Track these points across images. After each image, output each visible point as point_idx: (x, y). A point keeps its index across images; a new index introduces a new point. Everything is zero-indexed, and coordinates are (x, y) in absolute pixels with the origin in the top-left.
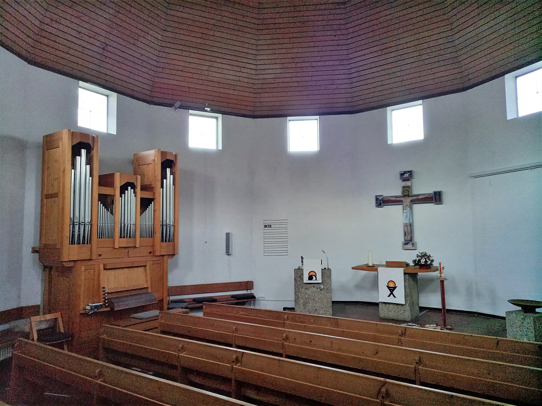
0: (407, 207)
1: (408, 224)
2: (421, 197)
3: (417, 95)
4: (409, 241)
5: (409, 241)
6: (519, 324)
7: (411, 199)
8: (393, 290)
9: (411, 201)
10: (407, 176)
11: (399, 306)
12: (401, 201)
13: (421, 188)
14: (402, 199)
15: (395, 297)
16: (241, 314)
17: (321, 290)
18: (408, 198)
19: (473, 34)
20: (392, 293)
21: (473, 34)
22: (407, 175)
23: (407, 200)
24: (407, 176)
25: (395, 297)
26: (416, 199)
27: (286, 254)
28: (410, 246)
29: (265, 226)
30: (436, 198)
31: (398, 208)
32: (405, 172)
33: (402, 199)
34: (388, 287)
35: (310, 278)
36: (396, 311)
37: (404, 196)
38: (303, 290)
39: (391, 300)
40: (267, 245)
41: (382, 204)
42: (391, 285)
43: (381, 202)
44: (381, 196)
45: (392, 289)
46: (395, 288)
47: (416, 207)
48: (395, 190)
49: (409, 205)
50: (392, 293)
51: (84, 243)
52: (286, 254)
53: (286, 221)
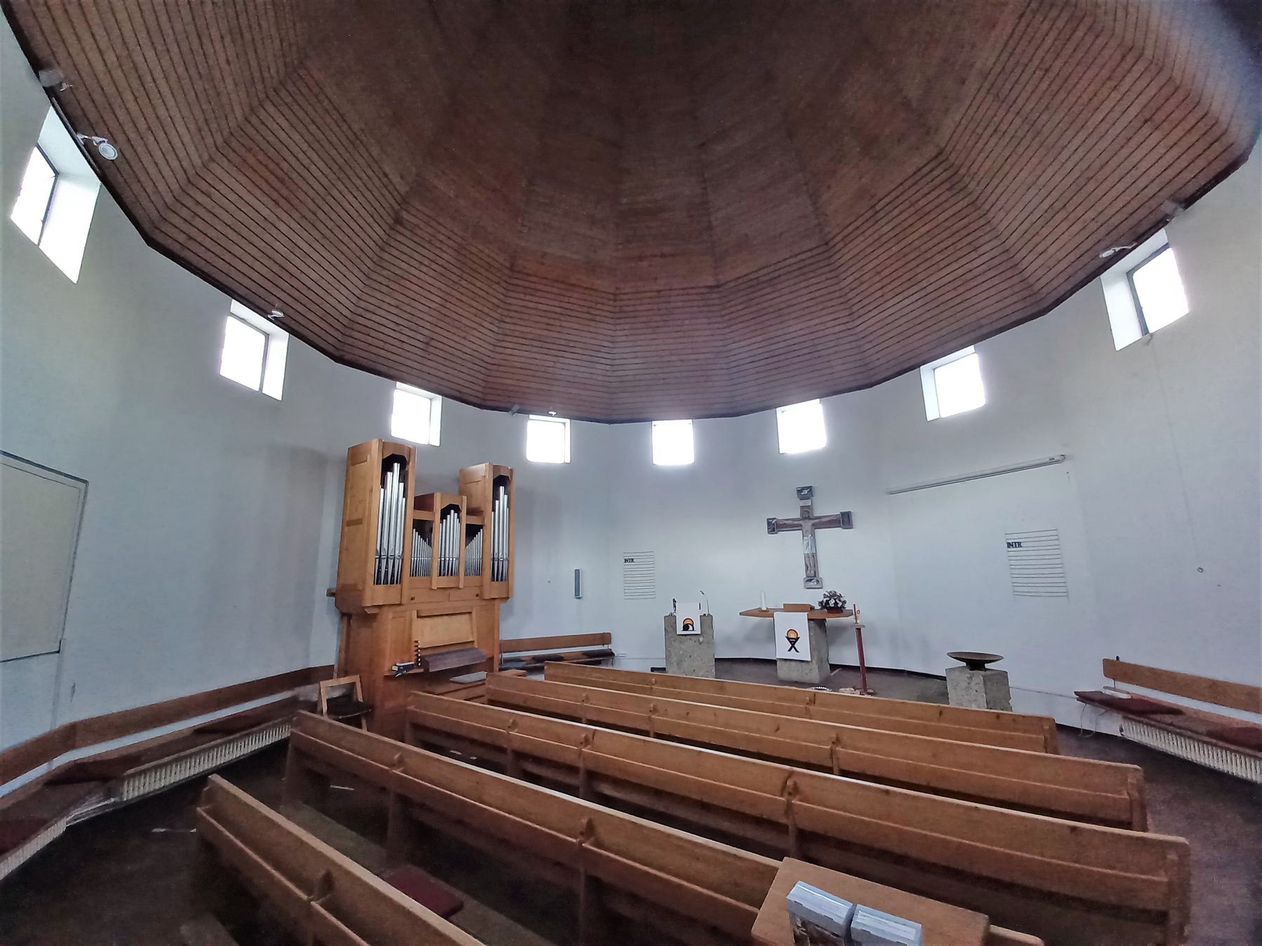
4: (812, 577)
5: (812, 577)
13: (825, 508)
18: (809, 521)
20: (793, 646)
23: (808, 525)
24: (806, 493)
30: (844, 520)
32: (803, 489)
35: (686, 627)
37: (804, 519)
39: (793, 655)
42: (793, 636)
43: (774, 527)
45: (793, 642)
50: (793, 646)
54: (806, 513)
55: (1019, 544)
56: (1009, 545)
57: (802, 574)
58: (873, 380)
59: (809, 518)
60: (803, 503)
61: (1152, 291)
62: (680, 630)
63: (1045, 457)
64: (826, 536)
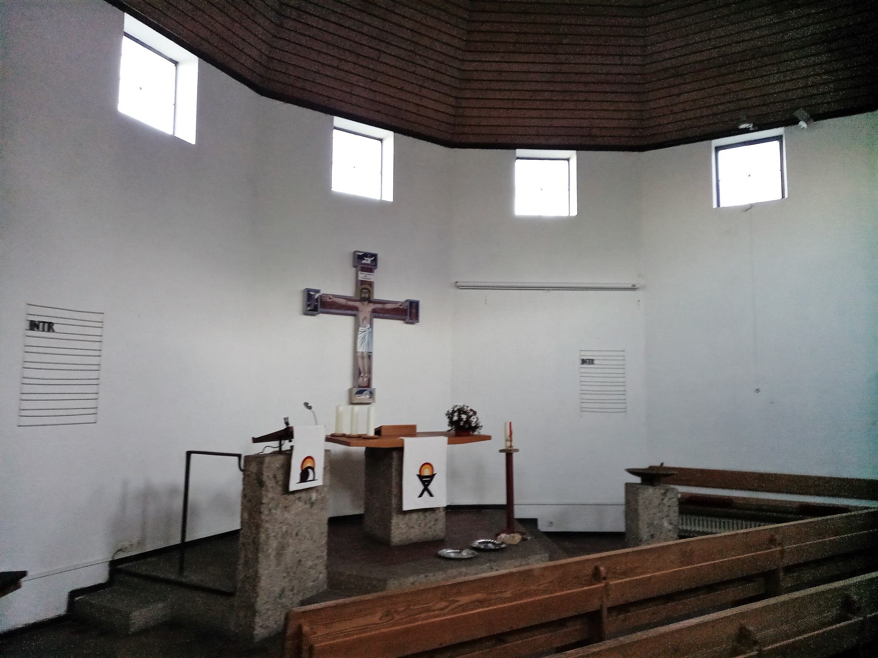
0: (365, 322)
1: (365, 354)
2: (389, 306)
3: (572, 141)
4: (362, 388)
5: (362, 388)
6: (656, 502)
7: (372, 306)
8: (429, 482)
9: (374, 311)
10: (365, 262)
11: (427, 514)
12: (356, 309)
13: (388, 289)
14: (357, 304)
15: (431, 495)
16: (464, 607)
17: (312, 504)
18: (363, 304)
19: (495, 67)
20: (426, 489)
21: (495, 67)
22: (368, 261)
23: (366, 309)
24: (365, 262)
25: (431, 495)
26: (381, 309)
27: (91, 419)
28: (365, 397)
29: (34, 325)
30: (409, 312)
31: (345, 322)
32: (366, 255)
33: (357, 304)
34: (421, 477)
35: (304, 477)
36: (423, 524)
37: (362, 300)
38: (278, 512)
39: (426, 502)
40: (587, 397)
41: (320, 309)
42: (427, 472)
43: (316, 304)
44: (318, 291)
45: (426, 480)
46: (432, 476)
47: (380, 324)
48: (340, 284)
49: (368, 317)
50: (426, 489)
51: (98, 367)
52: (91, 419)
53: (98, 318)
54: (365, 290)
55: (50, 327)
56: (34, 325)
57: (346, 382)
58: (456, 139)
59: (369, 300)
60: (362, 276)
61: (749, 170)
62: (295, 484)
63: (628, 283)
64: (384, 327)
